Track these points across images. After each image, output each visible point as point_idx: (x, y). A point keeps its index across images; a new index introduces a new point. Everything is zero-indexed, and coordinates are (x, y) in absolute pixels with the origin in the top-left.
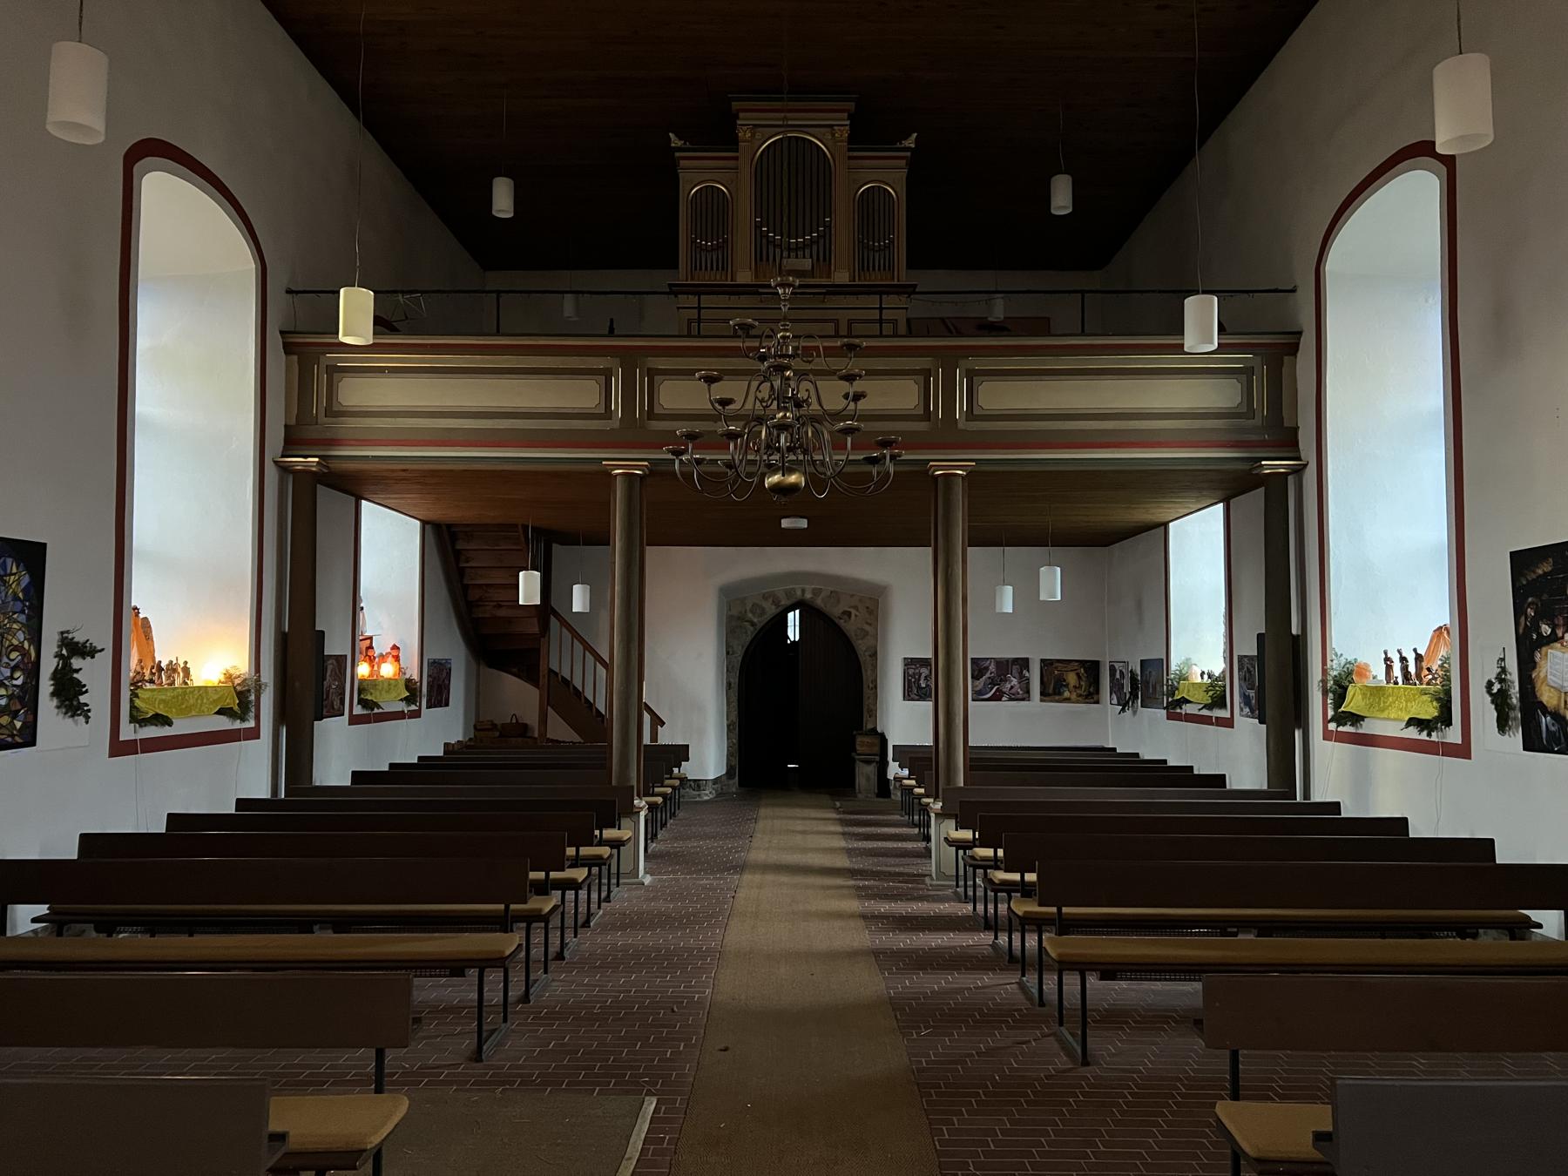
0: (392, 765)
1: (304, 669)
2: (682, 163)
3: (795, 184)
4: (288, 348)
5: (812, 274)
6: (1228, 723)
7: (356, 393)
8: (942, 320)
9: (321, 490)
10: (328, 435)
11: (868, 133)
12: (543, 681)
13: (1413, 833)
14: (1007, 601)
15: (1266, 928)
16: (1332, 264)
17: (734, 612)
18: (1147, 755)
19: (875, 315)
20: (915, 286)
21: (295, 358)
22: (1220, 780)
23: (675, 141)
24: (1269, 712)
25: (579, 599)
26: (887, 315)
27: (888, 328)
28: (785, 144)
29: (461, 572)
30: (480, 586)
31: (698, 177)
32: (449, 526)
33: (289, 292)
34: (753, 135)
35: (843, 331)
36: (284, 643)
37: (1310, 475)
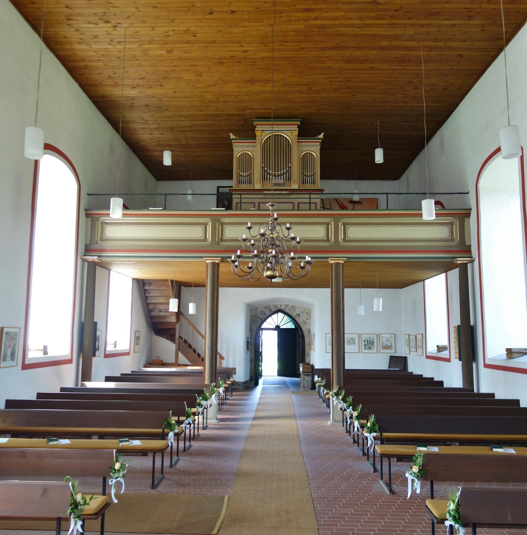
0: (39, 395)
1: (88, 337)
2: (235, 144)
3: (277, 149)
4: (87, 215)
5: (284, 185)
6: (448, 360)
7: (111, 232)
8: (336, 199)
9: (97, 268)
10: (101, 248)
11: (305, 133)
12: (177, 341)
13: (435, 380)
14: (362, 311)
15: (463, 442)
16: (482, 184)
17: (253, 314)
18: (427, 375)
19: (308, 200)
20: (323, 190)
21: (90, 219)
22: (441, 383)
23: (232, 136)
24: (462, 356)
25: (192, 309)
26: (312, 200)
27: (313, 206)
28: (272, 141)
29: (146, 298)
30: (153, 303)
31: (240, 148)
32: (142, 280)
33: (88, 194)
34: (262, 134)
35: (296, 208)
36: (82, 327)
37: (476, 263)
